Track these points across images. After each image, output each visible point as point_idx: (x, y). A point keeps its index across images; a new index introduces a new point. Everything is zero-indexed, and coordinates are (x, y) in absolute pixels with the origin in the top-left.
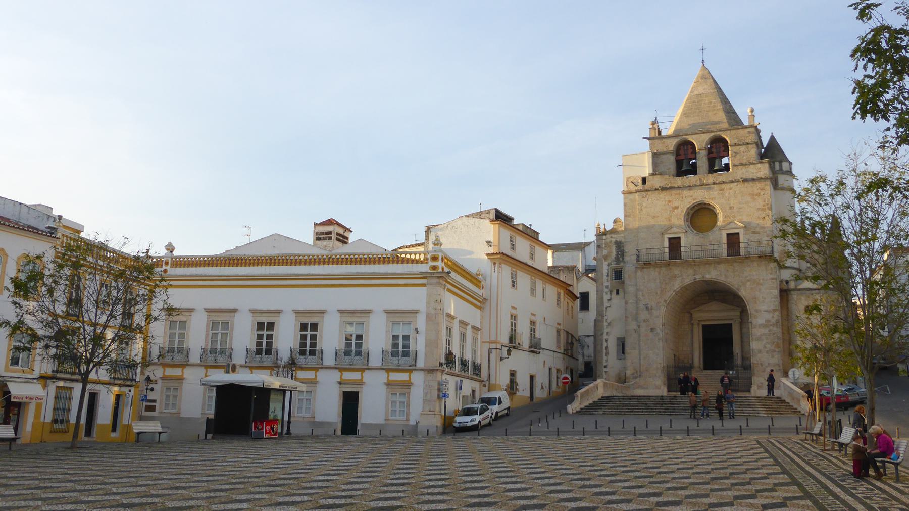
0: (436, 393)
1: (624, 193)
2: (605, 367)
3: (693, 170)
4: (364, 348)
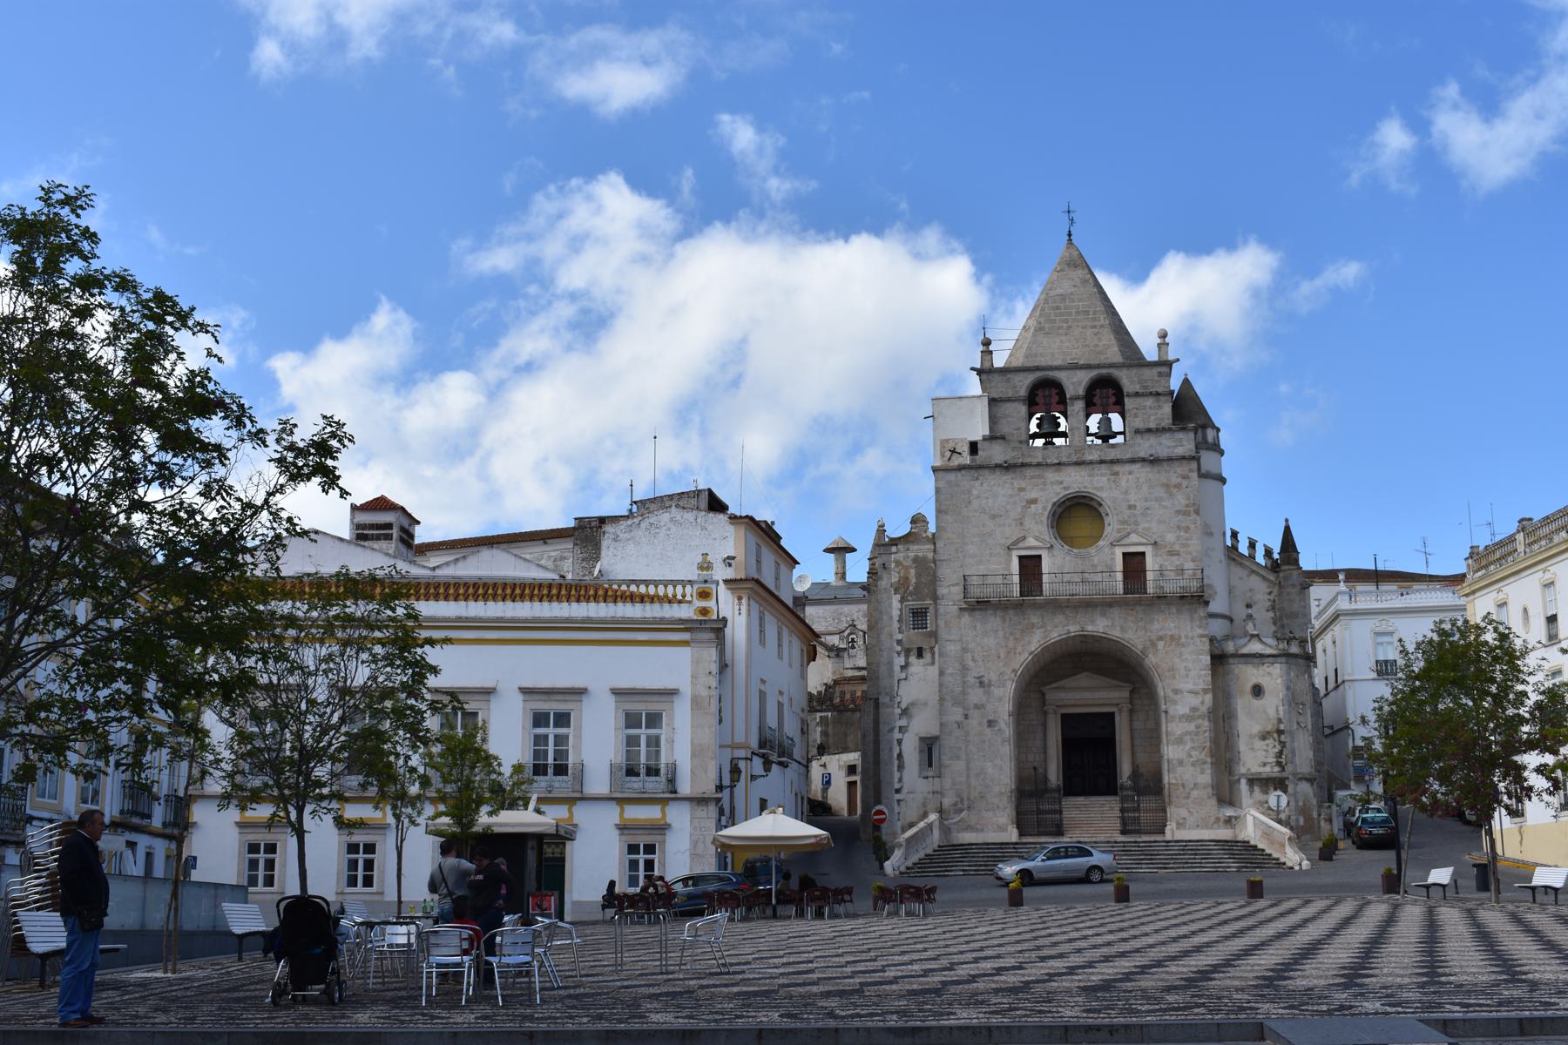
1: (935, 470)
2: (898, 791)
4: (664, 759)
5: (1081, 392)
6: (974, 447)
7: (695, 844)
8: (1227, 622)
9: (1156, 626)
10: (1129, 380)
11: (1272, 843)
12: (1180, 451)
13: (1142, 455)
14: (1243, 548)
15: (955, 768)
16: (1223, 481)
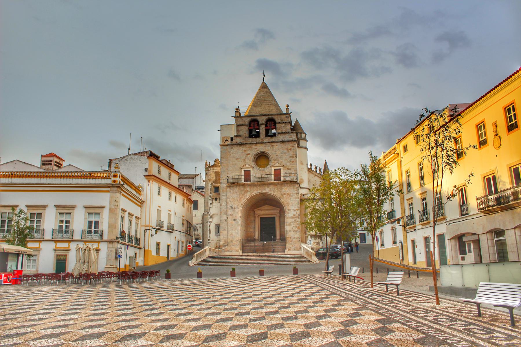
0: (114, 255)
2: (209, 240)
3: (258, 135)
5: (264, 122)
6: (232, 139)
7: (108, 256)
8: (308, 190)
9: (283, 190)
10: (277, 119)
11: (308, 255)
12: (291, 139)
13: (280, 140)
14: (313, 169)
15: (224, 233)
16: (307, 149)
